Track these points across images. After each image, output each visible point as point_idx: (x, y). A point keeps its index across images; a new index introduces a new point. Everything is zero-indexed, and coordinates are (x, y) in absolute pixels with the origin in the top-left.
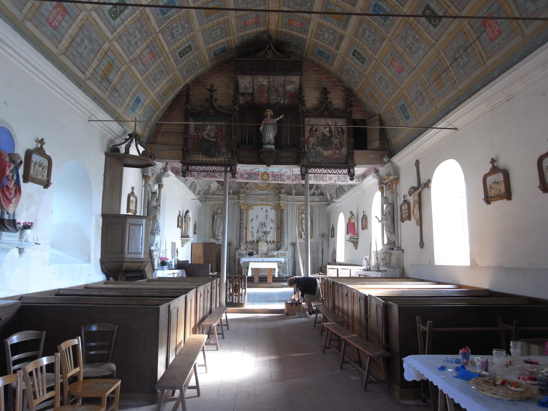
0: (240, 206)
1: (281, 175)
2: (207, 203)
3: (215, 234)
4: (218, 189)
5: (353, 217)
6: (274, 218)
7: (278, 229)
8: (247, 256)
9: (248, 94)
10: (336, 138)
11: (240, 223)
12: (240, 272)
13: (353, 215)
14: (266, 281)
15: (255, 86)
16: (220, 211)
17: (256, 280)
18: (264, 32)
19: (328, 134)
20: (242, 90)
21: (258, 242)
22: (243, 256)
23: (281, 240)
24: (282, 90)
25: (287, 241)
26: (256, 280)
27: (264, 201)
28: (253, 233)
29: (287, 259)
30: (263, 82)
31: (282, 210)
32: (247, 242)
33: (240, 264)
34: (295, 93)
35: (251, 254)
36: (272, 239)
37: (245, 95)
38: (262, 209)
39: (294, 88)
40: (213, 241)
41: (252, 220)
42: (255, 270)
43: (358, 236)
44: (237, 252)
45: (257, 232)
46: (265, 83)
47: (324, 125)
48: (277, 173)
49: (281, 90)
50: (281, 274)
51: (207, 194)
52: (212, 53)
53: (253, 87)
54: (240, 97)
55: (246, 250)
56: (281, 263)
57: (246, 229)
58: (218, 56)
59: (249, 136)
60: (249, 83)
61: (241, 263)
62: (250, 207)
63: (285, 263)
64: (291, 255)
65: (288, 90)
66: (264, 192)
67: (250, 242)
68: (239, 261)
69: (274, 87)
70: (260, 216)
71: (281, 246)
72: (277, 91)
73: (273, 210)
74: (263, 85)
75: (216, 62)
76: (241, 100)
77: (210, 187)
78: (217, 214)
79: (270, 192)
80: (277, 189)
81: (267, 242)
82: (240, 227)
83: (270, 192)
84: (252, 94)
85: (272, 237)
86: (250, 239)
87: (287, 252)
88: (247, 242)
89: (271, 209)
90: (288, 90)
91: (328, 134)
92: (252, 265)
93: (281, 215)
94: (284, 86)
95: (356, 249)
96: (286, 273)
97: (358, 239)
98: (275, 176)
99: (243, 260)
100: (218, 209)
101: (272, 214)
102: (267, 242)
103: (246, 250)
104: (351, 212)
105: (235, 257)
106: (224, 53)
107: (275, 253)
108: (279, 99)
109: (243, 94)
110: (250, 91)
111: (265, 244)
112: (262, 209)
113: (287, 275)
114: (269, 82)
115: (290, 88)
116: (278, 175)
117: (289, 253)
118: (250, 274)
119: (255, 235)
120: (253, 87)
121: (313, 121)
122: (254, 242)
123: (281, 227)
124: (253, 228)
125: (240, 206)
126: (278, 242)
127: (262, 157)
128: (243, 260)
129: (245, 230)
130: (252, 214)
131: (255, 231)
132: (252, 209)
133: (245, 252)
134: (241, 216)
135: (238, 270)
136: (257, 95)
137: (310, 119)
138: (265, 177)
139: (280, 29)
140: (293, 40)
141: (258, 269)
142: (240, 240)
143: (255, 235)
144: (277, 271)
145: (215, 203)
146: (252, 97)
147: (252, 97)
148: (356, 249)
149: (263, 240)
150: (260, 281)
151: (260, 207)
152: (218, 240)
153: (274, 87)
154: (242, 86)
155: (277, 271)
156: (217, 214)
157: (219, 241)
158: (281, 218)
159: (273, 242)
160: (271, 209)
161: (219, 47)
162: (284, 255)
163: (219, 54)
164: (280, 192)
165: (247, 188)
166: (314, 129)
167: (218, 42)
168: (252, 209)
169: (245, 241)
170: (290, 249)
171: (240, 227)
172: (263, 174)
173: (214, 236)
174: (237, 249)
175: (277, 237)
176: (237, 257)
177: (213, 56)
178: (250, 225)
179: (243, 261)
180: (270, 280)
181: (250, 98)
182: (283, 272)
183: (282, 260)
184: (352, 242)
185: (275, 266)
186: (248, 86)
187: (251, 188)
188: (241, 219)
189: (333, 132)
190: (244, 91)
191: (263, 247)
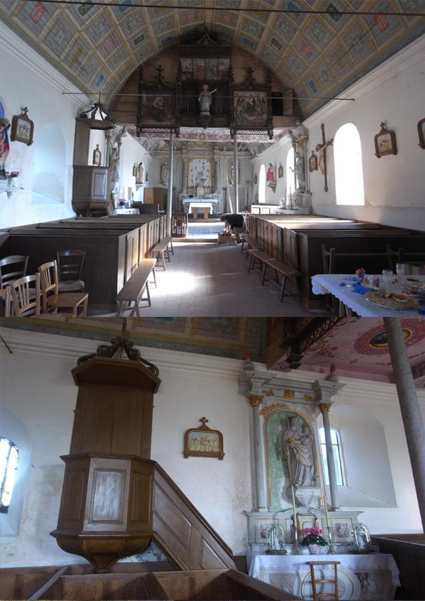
9: (189, 72)
10: (258, 106)
11: (183, 173)
12: (182, 210)
17: (195, 216)
20: (184, 70)
21: (196, 187)
22: (185, 198)
25: (220, 186)
26: (195, 216)
35: (191, 197)
36: (207, 185)
40: (160, 186)
41: (192, 170)
42: (194, 209)
47: (249, 97)
49: (215, 69)
50: (215, 212)
62: (190, 160)
66: (202, 148)
68: (182, 202)
72: (212, 70)
76: (184, 78)
78: (164, 165)
82: (183, 176)
84: (192, 73)
85: (208, 183)
86: (190, 184)
91: (252, 104)
92: (192, 205)
94: (217, 67)
95: (274, 192)
99: (185, 201)
100: (165, 161)
101: (208, 165)
104: (270, 164)
107: (210, 196)
109: (185, 73)
110: (191, 71)
115: (221, 68)
117: (221, 196)
119: (195, 182)
121: (240, 93)
128: (185, 201)
131: (194, 179)
142: (183, 185)
144: (212, 209)
148: (274, 192)
151: (198, 160)
155: (212, 209)
156: (164, 165)
162: (217, 197)
164: (214, 149)
166: (241, 100)
169: (186, 187)
170: (222, 192)
171: (183, 176)
173: (162, 183)
174: (180, 192)
175: (212, 183)
178: (190, 174)
180: (206, 216)
181: (190, 76)
183: (216, 201)
185: (210, 205)
188: (183, 169)
191: (201, 191)
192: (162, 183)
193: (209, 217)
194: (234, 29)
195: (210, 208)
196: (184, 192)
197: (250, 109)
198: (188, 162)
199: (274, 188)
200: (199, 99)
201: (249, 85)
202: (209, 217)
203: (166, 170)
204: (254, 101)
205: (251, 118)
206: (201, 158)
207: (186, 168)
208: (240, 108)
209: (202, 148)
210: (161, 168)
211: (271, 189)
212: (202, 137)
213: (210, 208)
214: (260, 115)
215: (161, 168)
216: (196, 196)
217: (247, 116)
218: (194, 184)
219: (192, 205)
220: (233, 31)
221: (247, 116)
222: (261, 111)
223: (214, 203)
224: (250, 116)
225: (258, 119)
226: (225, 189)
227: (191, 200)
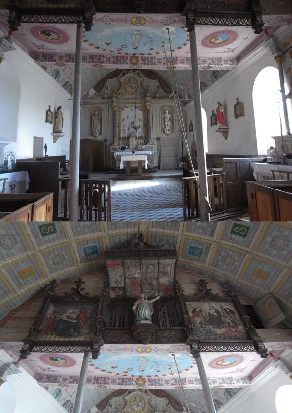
0: (113, 108)
1: (159, 380)
2: (86, 106)
3: (93, 133)
4: (95, 94)
5: (222, 107)
6: (141, 118)
7: (145, 126)
8: (120, 150)
9: (120, 288)
10: (226, 317)
11: (114, 122)
12: (114, 163)
13: (221, 105)
14: (137, 172)
15: (127, 280)
16: (96, 113)
17: (128, 171)
18: (134, 236)
19: (216, 314)
20: (113, 285)
21: (128, 138)
22: (116, 150)
23: (148, 136)
24: (156, 283)
25: (154, 135)
26: (128, 171)
27: (133, 104)
28: (124, 130)
29: (153, 152)
30: (135, 273)
31: (148, 111)
32: (119, 138)
33: (114, 157)
34: (170, 285)
35: (123, 149)
36: (140, 136)
37: (117, 290)
38: (131, 110)
39: (169, 280)
40: (91, 138)
41: (124, 119)
42: (127, 163)
43: (227, 126)
44: (111, 147)
45: (128, 130)
46: (137, 276)
47: (208, 308)
48: (153, 377)
49: (155, 283)
50: (149, 164)
51: (87, 98)
52: (83, 250)
53: (125, 280)
54: (111, 292)
55: (119, 145)
56: (149, 155)
57: (119, 127)
58: (89, 257)
59: (120, 320)
60: (120, 276)
61: (115, 156)
62: (122, 109)
63: (152, 155)
64: (156, 149)
65: (162, 283)
66: (133, 96)
67: (122, 138)
68: (113, 155)
69: (147, 280)
70: (130, 116)
71: (148, 141)
72: (150, 284)
73: (141, 111)
74: (135, 278)
75: (87, 263)
76: (113, 295)
77: (88, 93)
78: (94, 115)
79: (137, 97)
80: (143, 93)
81: (136, 138)
82: (114, 126)
83: (137, 97)
84: (124, 289)
85: (140, 132)
86: (122, 135)
87: (154, 146)
88: (119, 138)
89: (139, 110)
90: (162, 283)
91: (216, 314)
92: (124, 159)
93: (147, 115)
94: (158, 279)
95: (226, 138)
96: (153, 164)
97: (227, 128)
98: (152, 381)
99: (117, 153)
100: (95, 111)
101: (140, 114)
102: (136, 138)
103: (119, 145)
104: (219, 102)
105: (110, 151)
106: (96, 255)
107: (144, 147)
108: (153, 292)
109: (114, 289)
110: (122, 285)
111: (135, 139)
112: (131, 110)
113: (154, 166)
114: (142, 274)
115: (164, 280)
116: (155, 380)
117: (155, 147)
118: (122, 167)
119: (127, 132)
120: (125, 280)
121: (195, 305)
122: (125, 138)
123: (147, 124)
124: (124, 126)
125: (113, 108)
126: (146, 138)
127: (135, 333)
128: (117, 153)
129: (118, 128)
130: (123, 114)
131: (126, 128)
132: (123, 110)
133: (118, 147)
134: (114, 116)
135: (112, 163)
136: (129, 289)
137: (191, 303)
138: (141, 382)
139: (150, 230)
140: (164, 243)
141: (130, 161)
142: (114, 137)
143: (127, 132)
144: (147, 163)
145: (92, 106)
146: (124, 292)
147: (124, 292)
148: (226, 138)
149: (133, 136)
150: (131, 172)
151: (130, 109)
152: (96, 137)
153: (147, 280)
154: (113, 280)
155: (147, 163)
156: (94, 115)
157: (97, 138)
158: (147, 117)
159: (142, 137)
160: (139, 110)
161: (90, 245)
162: (151, 148)
163: (89, 255)
164: (146, 96)
165: (119, 94)
166: (197, 310)
167: (88, 236)
168: (123, 110)
169: (118, 138)
170: (156, 143)
171: (114, 126)
172: (137, 379)
173: (92, 134)
174: (111, 144)
175: (145, 134)
176: (112, 151)
177: (84, 255)
178: (122, 124)
179: (117, 154)
180: (140, 171)
181: (121, 292)
182: (150, 163)
183: (150, 152)
184: (222, 132)
185: (145, 158)
186: (119, 279)
187: (122, 93)
188: (114, 119)
189: (222, 313)
190: (115, 285)
191: (133, 142)
192: (92, 135)
193: (143, 172)
194: (176, 233)
195: (144, 161)
196: (116, 143)
197: (216, 320)
198: (119, 112)
199: (225, 133)
200: (134, 308)
201: (203, 294)
202: (143, 172)
203: (96, 120)
204: (217, 311)
205: (219, 331)
206: (132, 107)
207: (117, 117)
208: (198, 320)
209: (133, 96)
210: (91, 118)
211: (221, 135)
212: (141, 382)
213: (144, 161)
214: (233, 327)
215: (91, 118)
216: (129, 147)
217: (212, 328)
218: (126, 135)
219: (124, 159)
220: (175, 238)
221: (212, 328)
222: (233, 322)
223: (148, 155)
224: (218, 327)
225: (231, 331)
226: (158, 139)
227: (124, 152)
